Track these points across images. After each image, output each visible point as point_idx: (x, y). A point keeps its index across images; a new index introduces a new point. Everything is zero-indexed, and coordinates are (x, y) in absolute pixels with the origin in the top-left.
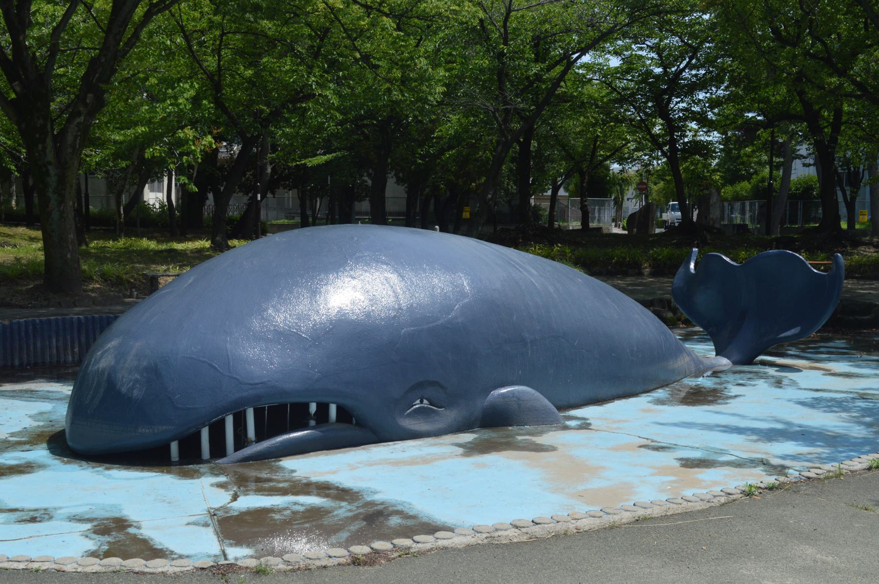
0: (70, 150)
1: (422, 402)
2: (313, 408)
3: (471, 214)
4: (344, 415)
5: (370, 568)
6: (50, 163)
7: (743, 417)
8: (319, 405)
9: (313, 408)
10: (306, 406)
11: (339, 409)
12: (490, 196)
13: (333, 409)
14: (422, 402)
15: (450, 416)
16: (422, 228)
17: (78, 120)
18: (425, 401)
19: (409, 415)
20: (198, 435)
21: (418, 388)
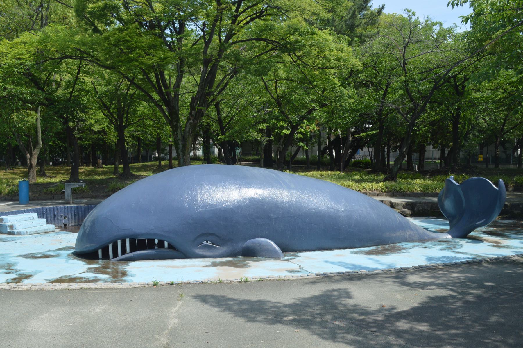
0: (187, 134)
1: (207, 242)
2: (156, 241)
3: (483, 158)
4: (170, 246)
5: (421, 290)
6: (179, 140)
7: (466, 253)
8: (159, 241)
9: (156, 241)
10: (154, 240)
11: (169, 244)
12: (404, 150)
13: (166, 244)
14: (207, 242)
15: (223, 249)
16: (228, 164)
17: (190, 122)
18: (209, 242)
19: (200, 248)
20: (98, 252)
21: (207, 235)
